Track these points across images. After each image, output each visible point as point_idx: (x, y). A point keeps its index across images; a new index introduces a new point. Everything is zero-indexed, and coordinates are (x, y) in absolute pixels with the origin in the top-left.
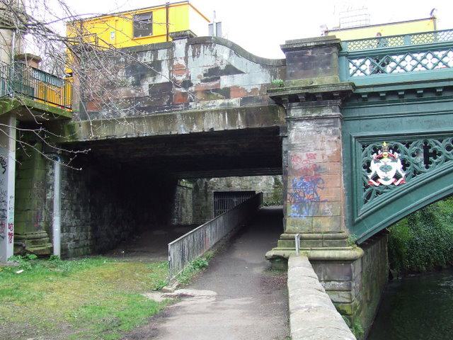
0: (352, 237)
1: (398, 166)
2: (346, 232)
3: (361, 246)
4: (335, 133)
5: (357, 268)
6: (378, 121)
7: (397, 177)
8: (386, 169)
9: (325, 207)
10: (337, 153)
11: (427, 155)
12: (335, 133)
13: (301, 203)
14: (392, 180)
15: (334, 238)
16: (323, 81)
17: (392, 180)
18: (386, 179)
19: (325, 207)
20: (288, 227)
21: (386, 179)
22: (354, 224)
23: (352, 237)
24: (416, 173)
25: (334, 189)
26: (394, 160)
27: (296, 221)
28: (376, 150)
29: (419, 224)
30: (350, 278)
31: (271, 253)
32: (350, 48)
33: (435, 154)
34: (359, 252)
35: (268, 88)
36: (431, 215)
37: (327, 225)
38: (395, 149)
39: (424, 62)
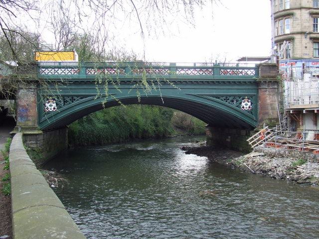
0: (39, 128)
1: (54, 105)
2: (37, 126)
3: (43, 130)
4: (34, 94)
5: (41, 138)
6: (47, 89)
7: (54, 108)
8: (51, 106)
9: (30, 118)
10: (35, 100)
11: (64, 102)
12: (34, 94)
13: (22, 117)
14: (53, 110)
15: (32, 128)
16: (30, 76)
17: (53, 110)
18: (51, 109)
19: (30, 118)
20: (17, 124)
21: (246, 108)
22: (40, 123)
23: (39, 128)
24: (61, 107)
25: (33, 111)
26: (249, 102)
27: (20, 122)
28: (243, 99)
29: (85, 124)
30: (37, 140)
31: (11, 133)
32: (42, 64)
33: (67, 101)
34: (41, 132)
35: (12, 76)
36: (91, 120)
37: (30, 124)
38: (54, 99)
39: (65, 72)
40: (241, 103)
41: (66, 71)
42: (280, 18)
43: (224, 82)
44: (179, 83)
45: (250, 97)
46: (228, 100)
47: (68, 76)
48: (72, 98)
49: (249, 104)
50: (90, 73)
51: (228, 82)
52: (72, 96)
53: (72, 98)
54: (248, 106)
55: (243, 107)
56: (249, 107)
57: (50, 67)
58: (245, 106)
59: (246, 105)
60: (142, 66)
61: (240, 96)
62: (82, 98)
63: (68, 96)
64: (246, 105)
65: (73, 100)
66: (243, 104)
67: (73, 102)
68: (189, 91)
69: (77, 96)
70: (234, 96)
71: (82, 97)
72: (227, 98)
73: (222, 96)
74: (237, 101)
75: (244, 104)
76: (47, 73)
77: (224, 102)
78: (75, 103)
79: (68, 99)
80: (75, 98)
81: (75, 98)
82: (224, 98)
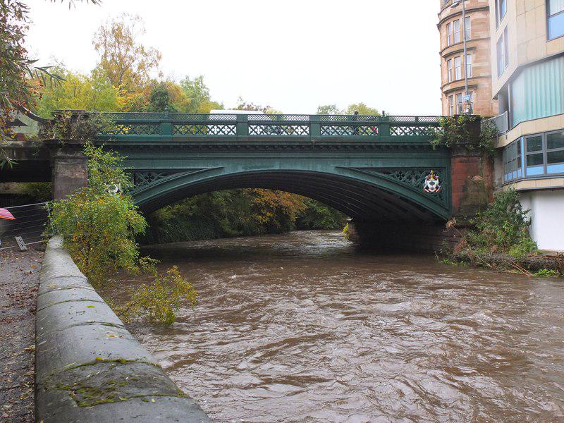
21: (432, 189)
40: (423, 181)
41: (226, 130)
42: (456, 55)
43: (354, 147)
44: (290, 149)
45: (438, 171)
46: (403, 176)
47: (342, 138)
48: (150, 174)
49: (437, 182)
50: (345, 134)
51: (270, 146)
52: (150, 171)
53: (150, 174)
54: (434, 186)
55: (427, 188)
56: (437, 188)
57: (143, 123)
58: (430, 186)
59: (431, 184)
60: (385, 122)
61: (421, 170)
62: (165, 175)
63: (142, 171)
64: (431, 184)
65: (150, 178)
66: (428, 183)
67: (150, 181)
68: (355, 164)
69: (158, 171)
70: (412, 169)
71: (167, 172)
72: (401, 172)
73: (394, 169)
74: (417, 178)
75: (429, 182)
76: (215, 133)
77: (397, 180)
78: (155, 182)
79: (142, 177)
80: (153, 174)
81: (153, 174)
82: (397, 173)
